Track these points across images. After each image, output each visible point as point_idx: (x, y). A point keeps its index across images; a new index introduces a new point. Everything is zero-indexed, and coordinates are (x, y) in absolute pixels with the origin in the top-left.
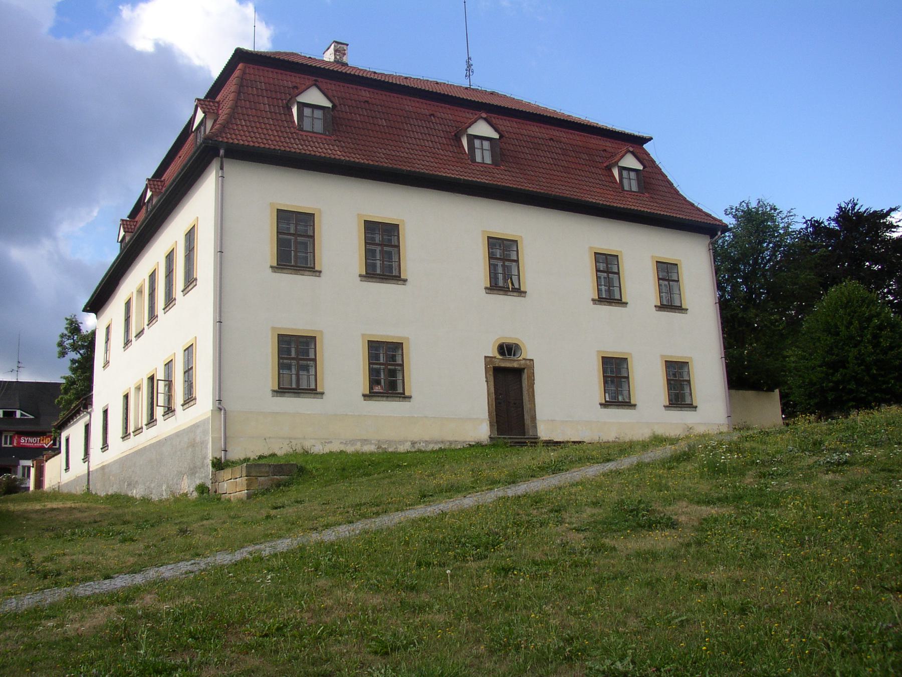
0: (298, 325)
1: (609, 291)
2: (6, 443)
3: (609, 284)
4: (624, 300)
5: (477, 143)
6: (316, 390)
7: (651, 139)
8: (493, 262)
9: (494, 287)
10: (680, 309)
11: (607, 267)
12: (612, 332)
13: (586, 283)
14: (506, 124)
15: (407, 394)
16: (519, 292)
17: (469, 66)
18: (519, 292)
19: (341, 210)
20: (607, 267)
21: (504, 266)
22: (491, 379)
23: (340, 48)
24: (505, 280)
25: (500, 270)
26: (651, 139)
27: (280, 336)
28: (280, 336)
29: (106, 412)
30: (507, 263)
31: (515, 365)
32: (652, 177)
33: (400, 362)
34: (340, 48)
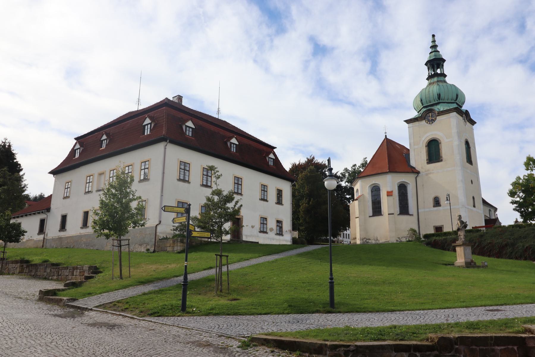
13: (258, 194)
20: (264, 188)
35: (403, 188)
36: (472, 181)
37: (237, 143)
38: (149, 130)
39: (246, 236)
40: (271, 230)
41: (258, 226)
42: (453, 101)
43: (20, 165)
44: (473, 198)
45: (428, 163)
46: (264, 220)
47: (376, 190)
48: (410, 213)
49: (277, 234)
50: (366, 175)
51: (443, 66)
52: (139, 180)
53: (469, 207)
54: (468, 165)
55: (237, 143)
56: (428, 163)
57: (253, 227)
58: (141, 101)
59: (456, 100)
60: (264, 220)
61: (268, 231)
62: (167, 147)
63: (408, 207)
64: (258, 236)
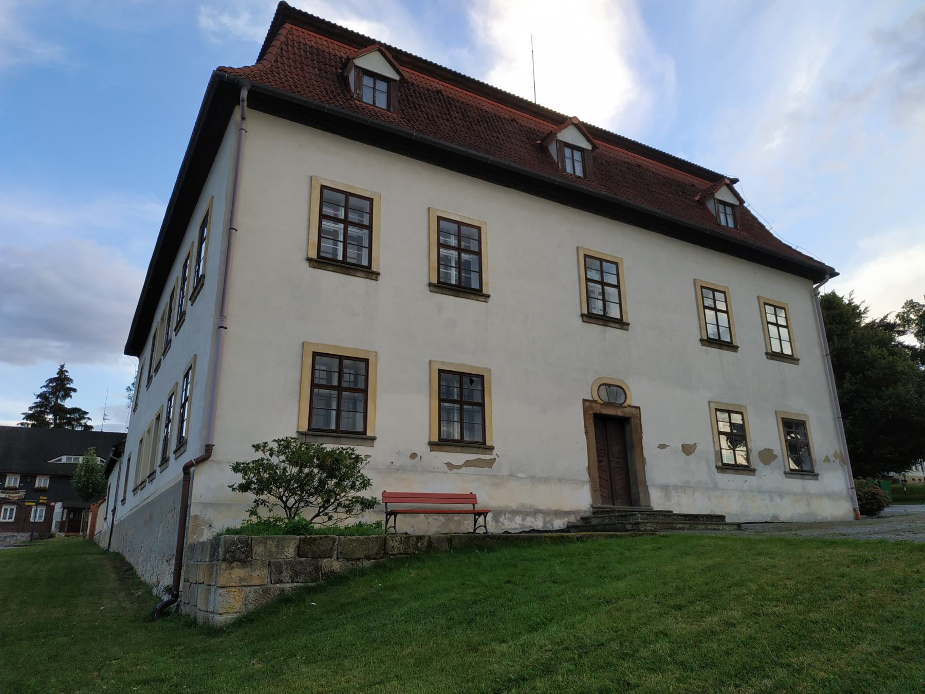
0: (343, 339)
2: (12, 510)
4: (374, 269)
5: (568, 152)
6: (365, 432)
10: (478, 294)
11: (599, 275)
14: (409, 73)
15: (369, 433)
22: (592, 429)
27: (441, 371)
28: (441, 371)
29: (129, 460)
33: (480, 401)
39: (665, 488)
57: (688, 449)
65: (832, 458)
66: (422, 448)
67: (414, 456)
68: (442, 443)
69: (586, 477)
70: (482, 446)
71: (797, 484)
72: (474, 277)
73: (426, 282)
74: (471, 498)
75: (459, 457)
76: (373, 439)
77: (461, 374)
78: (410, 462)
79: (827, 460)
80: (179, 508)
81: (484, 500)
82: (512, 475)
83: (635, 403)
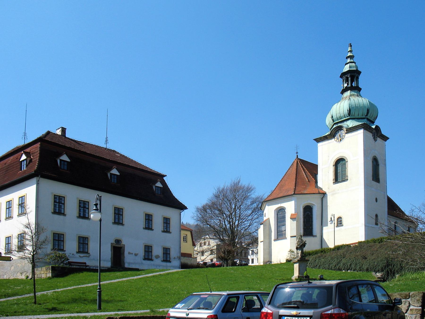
1: (149, 226)
3: (60, 207)
7: (166, 176)
8: (55, 203)
9: (115, 223)
10: (152, 229)
11: (149, 218)
12: (148, 237)
13: (142, 223)
16: (122, 224)
17: (107, 140)
18: (122, 224)
19: (73, 194)
20: (149, 218)
21: (59, 205)
23: (64, 130)
24: (118, 220)
25: (82, 211)
26: (166, 176)
27: (54, 233)
28: (54, 233)
30: (60, 204)
31: (119, 246)
32: (166, 189)
34: (64, 130)
35: (308, 211)
36: (376, 201)
37: (118, 174)
38: (25, 166)
39: (129, 263)
40: (157, 257)
41: (141, 253)
42: (364, 117)
43: (161, 177)
44: (377, 216)
45: (334, 183)
46: (148, 249)
47: (280, 214)
48: (314, 234)
49: (164, 261)
50: (272, 198)
51: (358, 78)
52: (17, 214)
53: (373, 226)
54: (374, 183)
55: (118, 174)
56: (334, 183)
57: (136, 255)
58: (28, 135)
59: (367, 115)
60: (148, 249)
61: (154, 258)
62: (40, 182)
63: (312, 228)
64: (142, 263)
65: (176, 257)
66: (75, 253)
67: (73, 254)
68: (79, 252)
69: (110, 260)
70: (87, 253)
71: (164, 264)
72: (63, 210)
73: (51, 212)
74: (85, 263)
75: (82, 255)
76: (65, 251)
77: (83, 237)
78: (72, 256)
79: (175, 258)
80: (130, 272)
81: (87, 264)
82: (94, 259)
83: (124, 244)
